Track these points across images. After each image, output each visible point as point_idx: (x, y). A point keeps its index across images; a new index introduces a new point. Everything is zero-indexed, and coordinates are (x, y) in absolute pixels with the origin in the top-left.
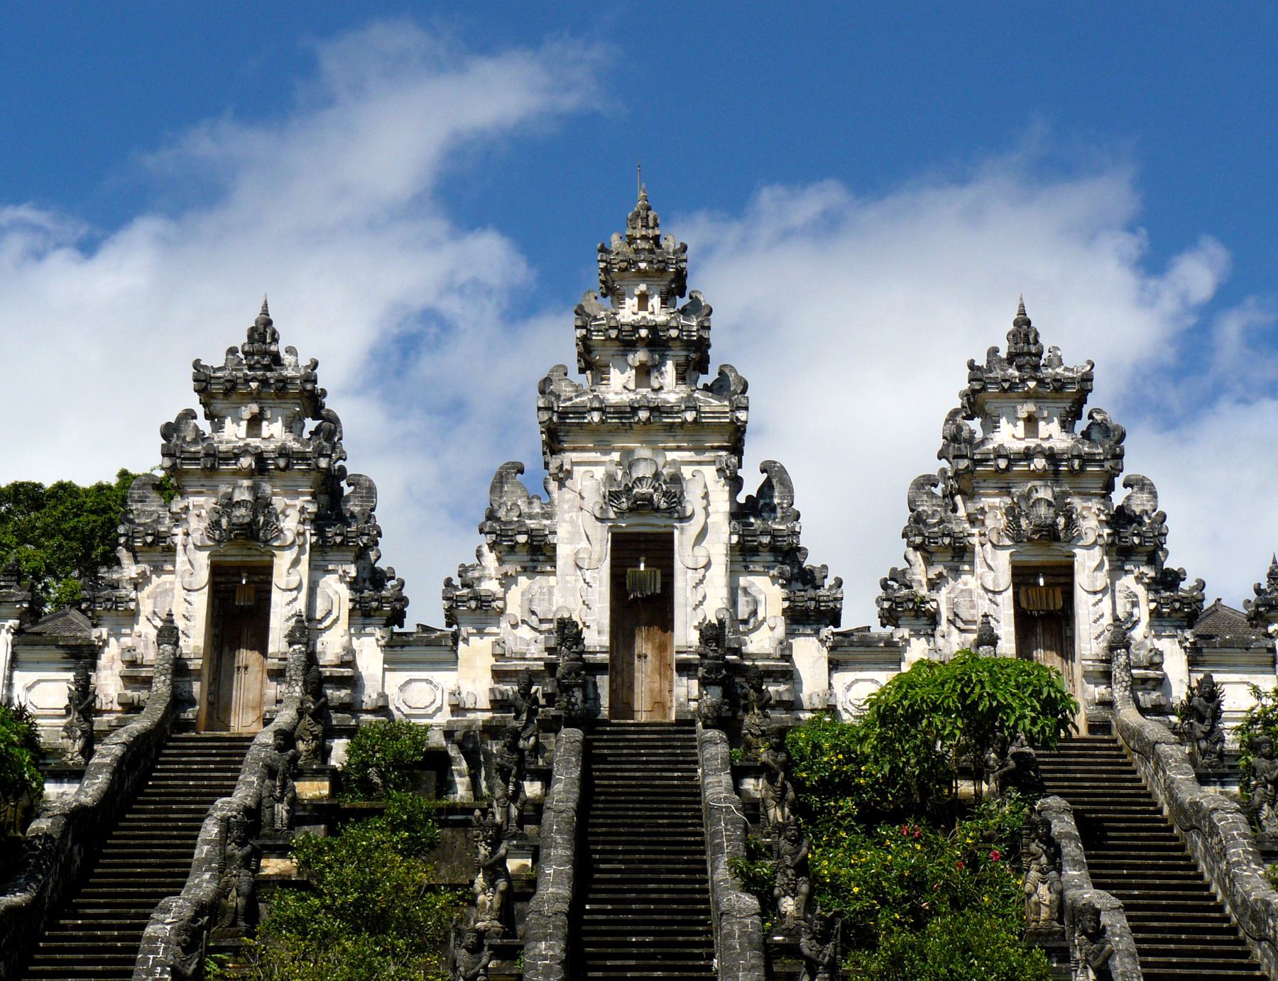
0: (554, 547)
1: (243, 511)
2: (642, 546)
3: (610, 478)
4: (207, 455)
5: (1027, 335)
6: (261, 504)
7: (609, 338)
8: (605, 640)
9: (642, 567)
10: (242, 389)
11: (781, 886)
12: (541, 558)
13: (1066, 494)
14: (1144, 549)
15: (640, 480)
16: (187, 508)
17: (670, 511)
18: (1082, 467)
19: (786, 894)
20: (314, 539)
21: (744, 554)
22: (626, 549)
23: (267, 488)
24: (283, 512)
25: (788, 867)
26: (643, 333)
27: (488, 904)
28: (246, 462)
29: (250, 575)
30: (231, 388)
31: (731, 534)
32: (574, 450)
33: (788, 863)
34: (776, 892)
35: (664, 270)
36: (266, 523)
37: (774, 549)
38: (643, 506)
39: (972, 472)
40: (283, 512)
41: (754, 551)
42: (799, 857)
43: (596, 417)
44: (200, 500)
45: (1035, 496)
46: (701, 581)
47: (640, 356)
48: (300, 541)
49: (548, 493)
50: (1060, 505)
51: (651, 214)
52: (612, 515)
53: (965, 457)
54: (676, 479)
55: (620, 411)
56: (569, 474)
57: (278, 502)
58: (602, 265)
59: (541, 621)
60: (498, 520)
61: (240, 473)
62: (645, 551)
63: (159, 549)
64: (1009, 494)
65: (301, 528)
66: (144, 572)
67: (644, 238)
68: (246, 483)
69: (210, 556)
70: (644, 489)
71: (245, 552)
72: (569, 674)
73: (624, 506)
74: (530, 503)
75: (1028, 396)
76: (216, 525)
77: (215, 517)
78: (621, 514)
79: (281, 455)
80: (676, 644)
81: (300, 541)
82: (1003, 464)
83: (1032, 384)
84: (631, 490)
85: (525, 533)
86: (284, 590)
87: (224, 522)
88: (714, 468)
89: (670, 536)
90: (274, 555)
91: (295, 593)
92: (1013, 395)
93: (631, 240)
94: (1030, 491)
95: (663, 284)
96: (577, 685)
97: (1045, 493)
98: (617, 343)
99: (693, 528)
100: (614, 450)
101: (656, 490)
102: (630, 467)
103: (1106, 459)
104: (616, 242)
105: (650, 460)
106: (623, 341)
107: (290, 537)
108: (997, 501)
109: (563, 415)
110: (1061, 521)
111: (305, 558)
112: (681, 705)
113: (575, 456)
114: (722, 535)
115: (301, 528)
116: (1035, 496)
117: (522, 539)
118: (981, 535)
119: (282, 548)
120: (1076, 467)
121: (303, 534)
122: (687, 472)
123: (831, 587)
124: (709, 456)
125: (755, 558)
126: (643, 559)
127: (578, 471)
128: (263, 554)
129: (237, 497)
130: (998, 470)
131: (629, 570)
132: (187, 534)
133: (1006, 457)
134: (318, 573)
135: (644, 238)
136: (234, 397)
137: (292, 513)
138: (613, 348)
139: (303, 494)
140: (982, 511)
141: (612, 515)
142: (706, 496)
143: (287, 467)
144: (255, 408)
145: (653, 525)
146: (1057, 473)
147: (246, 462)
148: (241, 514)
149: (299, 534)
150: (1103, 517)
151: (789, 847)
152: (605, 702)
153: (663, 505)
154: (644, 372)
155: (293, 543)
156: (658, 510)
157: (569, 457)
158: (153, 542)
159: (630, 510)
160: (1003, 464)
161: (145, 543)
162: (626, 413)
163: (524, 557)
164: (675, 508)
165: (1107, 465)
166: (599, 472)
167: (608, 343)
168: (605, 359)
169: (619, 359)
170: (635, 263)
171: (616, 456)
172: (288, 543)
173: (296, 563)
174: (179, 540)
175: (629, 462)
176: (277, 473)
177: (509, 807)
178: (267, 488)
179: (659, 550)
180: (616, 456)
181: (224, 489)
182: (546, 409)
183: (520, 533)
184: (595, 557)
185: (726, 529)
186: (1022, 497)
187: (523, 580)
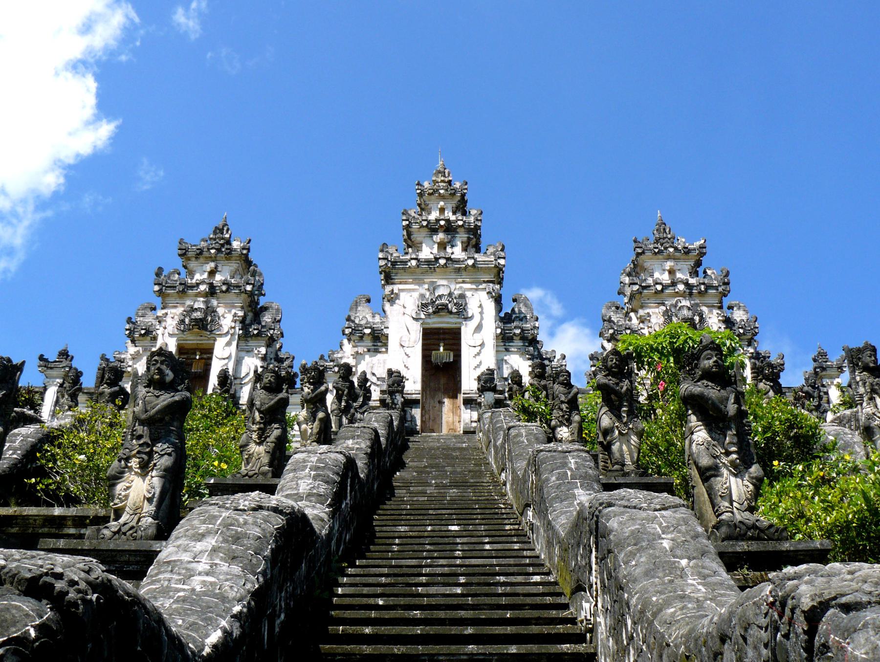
0: (387, 336)
1: (199, 313)
2: (442, 336)
3: (422, 296)
4: (181, 284)
5: (664, 229)
6: (210, 311)
7: (422, 226)
8: (418, 387)
9: (442, 349)
10: (206, 254)
11: (557, 418)
12: (379, 344)
13: (697, 305)
14: (745, 337)
15: (440, 297)
16: (167, 314)
17: (458, 313)
18: (706, 289)
19: (562, 424)
20: (241, 332)
21: (504, 339)
22: (431, 338)
23: (214, 302)
24: (223, 316)
25: (562, 402)
26: (442, 223)
27: (310, 431)
28: (203, 288)
29: (201, 353)
30: (200, 253)
31: (496, 328)
32: (401, 283)
33: (563, 398)
34: (553, 423)
35: (454, 194)
36: (212, 321)
37: (523, 338)
38: (440, 310)
39: (641, 293)
40: (223, 316)
41: (511, 339)
42: (570, 396)
43: (414, 263)
44: (173, 311)
45: (680, 305)
46: (478, 354)
47: (440, 236)
48: (232, 331)
49: (384, 311)
50: (693, 308)
51: (447, 171)
52: (423, 316)
53: (636, 284)
54: (462, 296)
55: (428, 262)
56: (397, 296)
57: (221, 311)
58: (418, 191)
59: (378, 379)
60: (353, 322)
61: (199, 295)
62: (444, 339)
63: (149, 338)
64: (663, 304)
65: (233, 324)
66: (138, 351)
67: (443, 181)
68: (202, 299)
69: (178, 340)
70: (444, 301)
71: (199, 338)
72: (393, 385)
73: (431, 311)
74: (374, 317)
75: (669, 258)
76: (182, 322)
77: (182, 317)
78: (428, 315)
79: (224, 284)
80: (463, 388)
81: (232, 331)
82: (659, 287)
83: (671, 250)
84: (434, 302)
85: (370, 328)
86: (220, 359)
87: (187, 321)
88: (485, 293)
89: (460, 329)
90: (215, 340)
91: (226, 361)
92: (661, 257)
93: (435, 182)
94: (677, 302)
95: (454, 203)
96: (398, 391)
97: (686, 303)
98: (426, 230)
99: (471, 325)
100: (424, 283)
101: (450, 302)
102: (434, 289)
103: (720, 286)
104: (426, 184)
105: (445, 287)
106: (431, 229)
107: (225, 329)
108: (657, 310)
109: (394, 263)
110: (697, 318)
111: (235, 343)
112: (467, 424)
113: (401, 287)
114: (491, 328)
115: (233, 324)
116: (680, 305)
117: (368, 331)
118: (649, 327)
119: (220, 335)
120: (703, 289)
121: (234, 328)
122: (468, 294)
123: (558, 360)
124: (484, 286)
125: (511, 344)
126: (442, 344)
127: (402, 295)
128: (209, 339)
129: (196, 306)
130: (657, 292)
131: (433, 352)
132: (165, 328)
133: (661, 284)
134: (242, 354)
135: (443, 181)
136: (202, 260)
137: (228, 318)
138: (425, 232)
139: (235, 307)
140: (649, 315)
141: (423, 316)
142: (481, 306)
143: (227, 291)
144: (212, 265)
145: (448, 323)
146: (691, 294)
147: (203, 288)
148: (198, 315)
149: (232, 328)
150: (720, 318)
151: (562, 389)
152: (419, 422)
153: (454, 310)
154: (442, 246)
155: (228, 332)
156: (451, 313)
157: (396, 288)
158: (145, 334)
159: (434, 312)
160: (659, 287)
161: (141, 335)
162: (431, 264)
163: (368, 342)
164: (462, 312)
165: (720, 289)
166: (416, 295)
167: (421, 230)
168: (419, 239)
169: (428, 240)
170: (438, 190)
171: (426, 286)
172: (225, 331)
173: (229, 344)
174: (159, 332)
175: (434, 288)
176: (222, 295)
177: (341, 417)
178: (214, 302)
179: (453, 338)
180: (426, 286)
181: (189, 303)
182: (384, 259)
183: (366, 328)
184: (412, 339)
185: (493, 325)
186: (671, 305)
187: (367, 357)
